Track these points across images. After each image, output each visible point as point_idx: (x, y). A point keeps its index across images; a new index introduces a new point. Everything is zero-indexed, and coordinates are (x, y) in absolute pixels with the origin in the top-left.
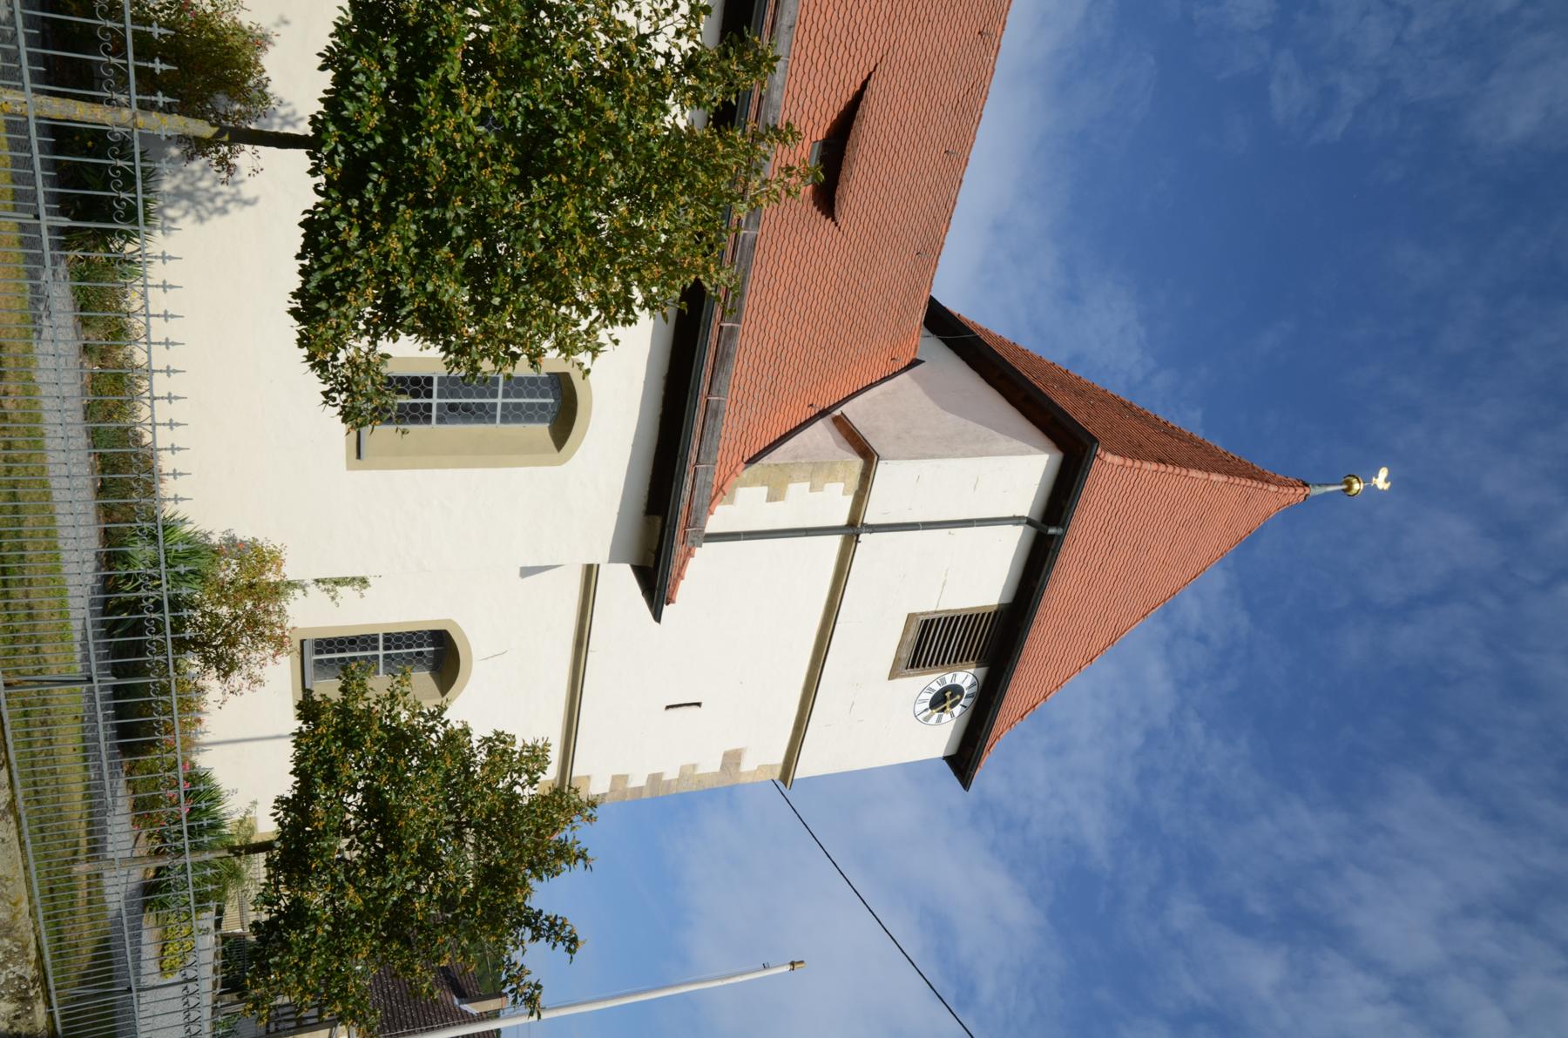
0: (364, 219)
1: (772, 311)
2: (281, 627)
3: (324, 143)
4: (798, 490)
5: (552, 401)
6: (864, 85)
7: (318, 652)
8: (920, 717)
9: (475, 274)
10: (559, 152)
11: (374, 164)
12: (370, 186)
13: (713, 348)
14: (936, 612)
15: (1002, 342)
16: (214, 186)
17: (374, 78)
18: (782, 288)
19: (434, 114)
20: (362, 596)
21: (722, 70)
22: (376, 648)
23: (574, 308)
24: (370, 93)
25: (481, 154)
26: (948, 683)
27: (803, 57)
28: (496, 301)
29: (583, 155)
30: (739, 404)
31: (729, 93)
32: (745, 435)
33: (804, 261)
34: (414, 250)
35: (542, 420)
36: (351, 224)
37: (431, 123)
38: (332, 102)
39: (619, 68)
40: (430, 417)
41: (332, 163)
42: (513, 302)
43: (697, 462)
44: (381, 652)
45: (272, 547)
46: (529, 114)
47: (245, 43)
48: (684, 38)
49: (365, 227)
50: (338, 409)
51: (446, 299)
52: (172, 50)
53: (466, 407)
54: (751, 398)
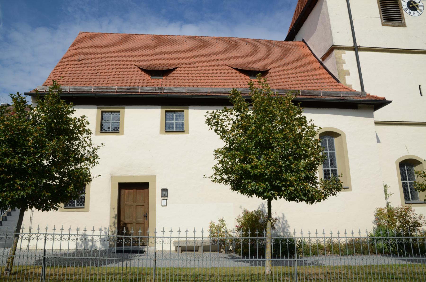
0: (287, 186)
1: (295, 82)
2: (402, 209)
3: (269, 196)
4: (345, 67)
5: (327, 138)
6: (234, 69)
7: (409, 199)
8: (420, 13)
9: (298, 158)
10: (264, 139)
11: (273, 184)
12: (279, 185)
13: (308, 96)
14: (381, 17)
15: (294, 18)
16: (280, 223)
17: (252, 185)
18: (289, 81)
19: (259, 170)
20: (390, 187)
21: (239, 102)
22: (407, 183)
23: (303, 133)
24: (256, 186)
25: (268, 158)
26: (407, 7)
27: (230, 85)
28: (304, 152)
29: (264, 134)
30: (322, 87)
31: (243, 100)
32: (331, 85)
33: (281, 76)
34: (293, 174)
35: (333, 140)
36: (289, 189)
37: (262, 171)
38: (259, 194)
39: (242, 127)
40: (335, 170)
41: (274, 194)
42: (303, 148)
43: (340, 96)
44: (408, 181)
45: (377, 211)
46: (256, 148)
47: (247, 215)
48: (233, 112)
49: (289, 186)
50: (337, 192)
51: (305, 165)
52: (253, 230)
53: (331, 160)
54: (320, 84)
